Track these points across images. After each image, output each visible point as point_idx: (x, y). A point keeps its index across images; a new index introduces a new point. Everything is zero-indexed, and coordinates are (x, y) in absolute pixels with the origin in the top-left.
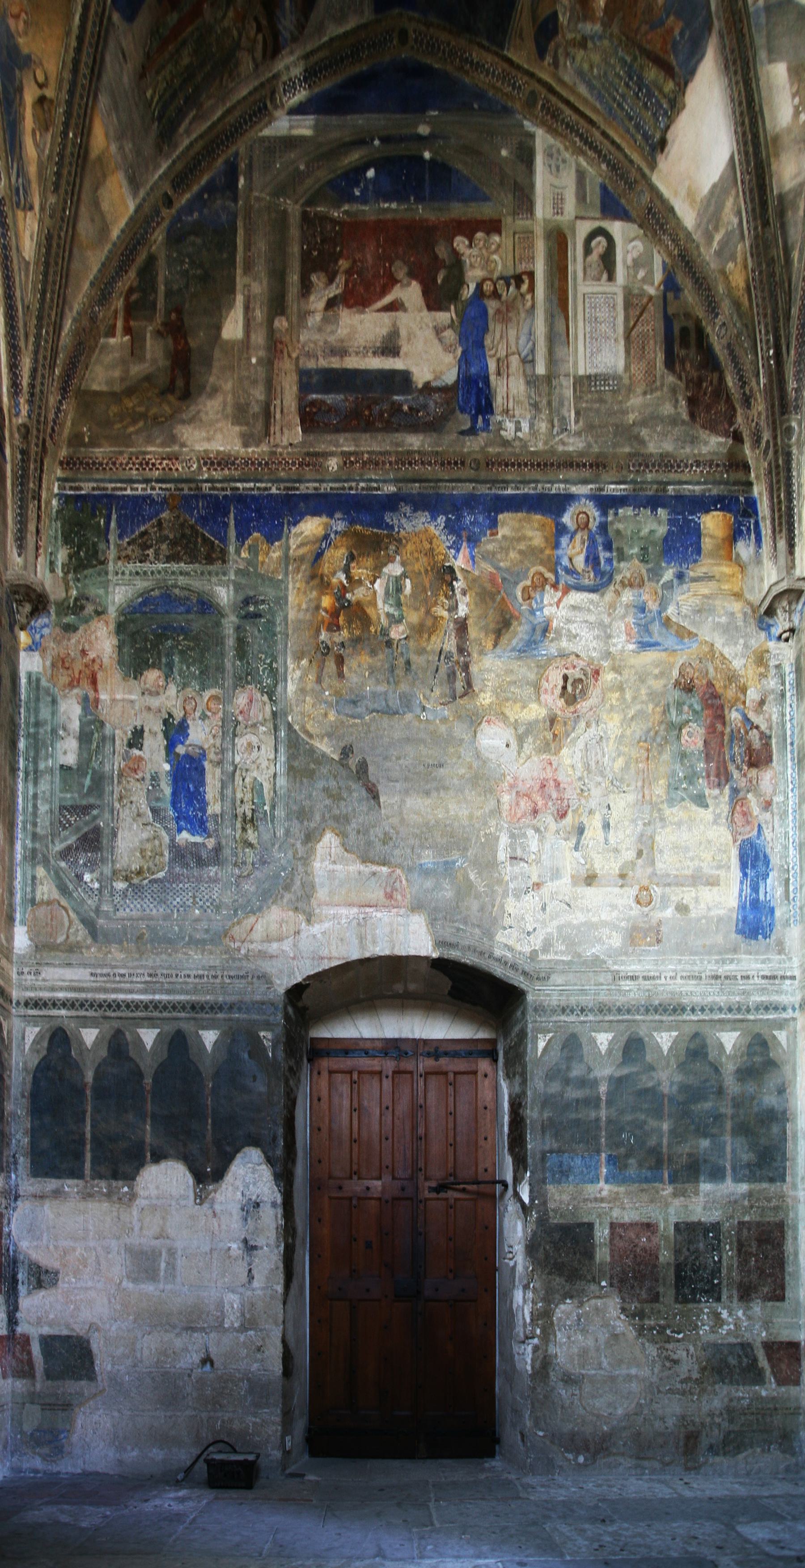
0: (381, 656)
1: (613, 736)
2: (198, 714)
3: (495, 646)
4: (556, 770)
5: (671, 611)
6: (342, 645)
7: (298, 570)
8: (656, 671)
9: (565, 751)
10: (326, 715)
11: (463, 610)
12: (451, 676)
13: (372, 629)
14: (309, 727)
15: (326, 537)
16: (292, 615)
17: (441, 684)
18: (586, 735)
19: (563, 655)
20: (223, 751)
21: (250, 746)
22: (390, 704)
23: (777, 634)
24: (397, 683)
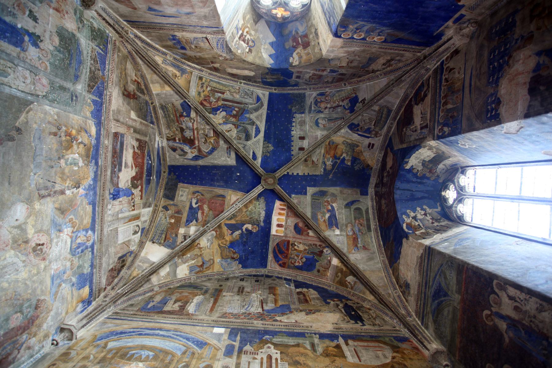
0: (56, 154)
1: (18, 276)
2: (41, 56)
3: (56, 208)
4: (4, 250)
5: (63, 285)
6: (60, 137)
7: (83, 122)
8: (44, 288)
9: (12, 252)
10: (36, 123)
11: (68, 192)
12: (46, 188)
13: (64, 151)
14: (31, 112)
15: (91, 136)
16: (71, 115)
17: (44, 183)
18: (20, 262)
19: (51, 241)
20: (24, 62)
21: (26, 78)
22: (38, 157)
23: (54, 338)
24: (45, 161)
